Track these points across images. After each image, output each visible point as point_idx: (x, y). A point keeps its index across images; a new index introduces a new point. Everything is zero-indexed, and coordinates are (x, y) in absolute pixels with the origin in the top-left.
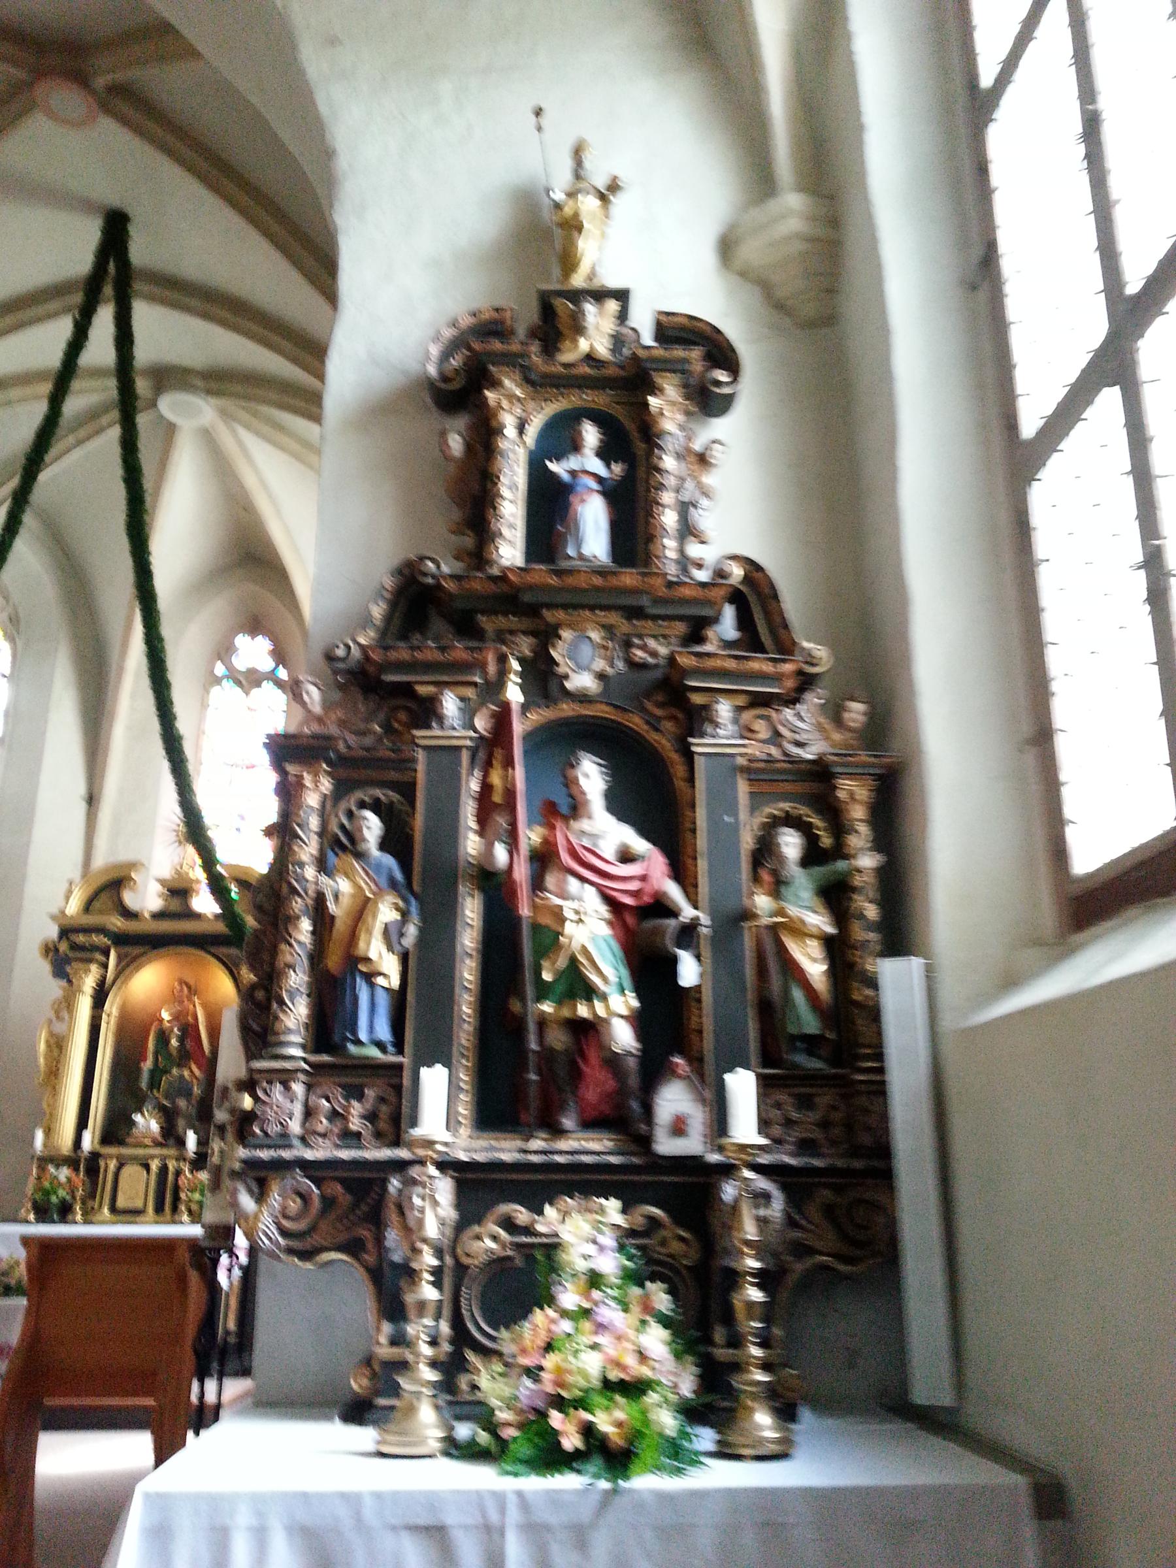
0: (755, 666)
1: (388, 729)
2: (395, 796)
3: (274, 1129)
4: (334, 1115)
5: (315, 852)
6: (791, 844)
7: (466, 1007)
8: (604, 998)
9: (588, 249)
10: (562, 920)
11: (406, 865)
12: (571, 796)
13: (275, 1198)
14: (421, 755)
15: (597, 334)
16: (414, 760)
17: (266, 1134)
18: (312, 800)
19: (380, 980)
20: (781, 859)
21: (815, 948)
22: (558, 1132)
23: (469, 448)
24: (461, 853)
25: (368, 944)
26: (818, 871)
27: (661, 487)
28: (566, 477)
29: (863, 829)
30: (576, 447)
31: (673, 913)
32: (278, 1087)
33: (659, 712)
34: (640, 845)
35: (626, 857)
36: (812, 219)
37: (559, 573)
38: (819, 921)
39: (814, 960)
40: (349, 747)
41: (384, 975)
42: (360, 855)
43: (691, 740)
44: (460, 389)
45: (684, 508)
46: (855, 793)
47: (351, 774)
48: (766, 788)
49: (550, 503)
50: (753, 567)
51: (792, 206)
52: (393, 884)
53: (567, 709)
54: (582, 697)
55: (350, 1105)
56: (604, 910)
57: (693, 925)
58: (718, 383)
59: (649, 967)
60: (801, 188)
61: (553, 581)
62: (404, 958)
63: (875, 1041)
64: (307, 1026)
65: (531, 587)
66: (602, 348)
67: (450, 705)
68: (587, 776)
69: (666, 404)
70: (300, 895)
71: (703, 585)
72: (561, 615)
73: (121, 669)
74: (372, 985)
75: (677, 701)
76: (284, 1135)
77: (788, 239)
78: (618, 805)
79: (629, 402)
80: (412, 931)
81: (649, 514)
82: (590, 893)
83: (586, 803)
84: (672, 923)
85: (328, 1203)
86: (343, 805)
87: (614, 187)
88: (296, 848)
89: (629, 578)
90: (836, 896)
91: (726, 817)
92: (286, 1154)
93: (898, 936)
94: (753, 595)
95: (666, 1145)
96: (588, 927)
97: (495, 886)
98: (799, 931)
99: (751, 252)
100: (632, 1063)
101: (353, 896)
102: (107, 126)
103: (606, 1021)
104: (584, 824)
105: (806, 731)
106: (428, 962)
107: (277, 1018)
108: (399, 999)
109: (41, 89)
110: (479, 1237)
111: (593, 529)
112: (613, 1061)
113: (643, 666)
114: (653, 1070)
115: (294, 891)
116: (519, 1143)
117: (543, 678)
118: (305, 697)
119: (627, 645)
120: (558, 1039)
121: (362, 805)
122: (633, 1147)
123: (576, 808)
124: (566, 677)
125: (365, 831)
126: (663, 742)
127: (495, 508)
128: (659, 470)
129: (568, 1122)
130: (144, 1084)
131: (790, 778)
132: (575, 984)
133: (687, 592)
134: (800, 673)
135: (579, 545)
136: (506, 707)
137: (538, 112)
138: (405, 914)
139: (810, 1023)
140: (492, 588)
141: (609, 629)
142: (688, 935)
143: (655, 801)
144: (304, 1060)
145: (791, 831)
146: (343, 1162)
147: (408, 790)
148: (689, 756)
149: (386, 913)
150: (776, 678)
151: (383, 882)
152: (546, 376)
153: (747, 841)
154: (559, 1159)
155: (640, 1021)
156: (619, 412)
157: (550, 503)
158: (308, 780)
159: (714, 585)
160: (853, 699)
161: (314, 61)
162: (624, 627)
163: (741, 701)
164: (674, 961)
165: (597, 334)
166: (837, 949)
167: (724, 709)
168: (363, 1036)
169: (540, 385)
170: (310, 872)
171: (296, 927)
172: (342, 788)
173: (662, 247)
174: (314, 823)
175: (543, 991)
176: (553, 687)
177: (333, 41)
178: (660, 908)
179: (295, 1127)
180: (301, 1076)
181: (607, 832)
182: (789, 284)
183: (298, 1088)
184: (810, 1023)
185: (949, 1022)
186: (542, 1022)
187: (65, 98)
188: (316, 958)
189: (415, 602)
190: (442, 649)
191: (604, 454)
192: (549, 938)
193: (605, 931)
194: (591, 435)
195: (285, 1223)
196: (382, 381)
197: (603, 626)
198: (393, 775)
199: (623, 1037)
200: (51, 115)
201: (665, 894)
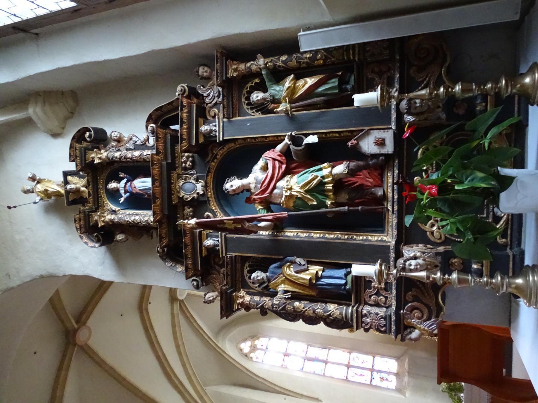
0: (185, 116)
1: (222, 266)
2: (247, 265)
3: (383, 322)
4: (378, 294)
5: (269, 298)
6: (257, 96)
7: (330, 236)
8: (323, 177)
9: (53, 187)
10: (291, 196)
11: (274, 261)
12: (242, 192)
13: (414, 322)
14: (229, 255)
15: (78, 183)
16: (231, 257)
17: (385, 326)
18: (248, 298)
19: (320, 273)
20: (264, 99)
21: (301, 82)
22: (385, 197)
23: (122, 232)
24: (267, 238)
25: (304, 279)
26: (268, 84)
27: (125, 158)
28: (128, 194)
29: (248, 65)
30: (117, 190)
31: (288, 146)
32: (364, 319)
33: (210, 155)
34: (261, 163)
35: (265, 168)
36: (36, 103)
37: (155, 198)
38: (288, 82)
39: (306, 83)
40: (227, 284)
41: (317, 272)
42: (269, 280)
43: (218, 141)
44: (104, 235)
45: (137, 147)
46: (236, 69)
47: (238, 282)
48: (236, 108)
49: (137, 201)
50: (149, 120)
51: (33, 111)
52: (280, 267)
53: (210, 194)
54: (206, 187)
55: (374, 287)
56: (287, 178)
57: (292, 138)
58: (90, 136)
59: (312, 156)
60: (27, 109)
61: (158, 202)
62: (309, 263)
63: (341, 51)
64: (339, 304)
65: (162, 210)
66: (84, 181)
67: (209, 242)
68: (232, 186)
69: (98, 156)
70: (286, 306)
71: (157, 140)
72: (174, 197)
74: (322, 277)
75: (205, 147)
76: (385, 318)
77: (45, 113)
78: (245, 173)
79: (98, 171)
80: (298, 260)
81: (137, 161)
82: (280, 184)
83: (243, 186)
84: (292, 147)
85: (415, 299)
86: (251, 285)
87: (33, 179)
88: (267, 307)
89: (155, 171)
90: (278, 75)
91: (249, 125)
92: (393, 318)
93: (290, 45)
94: (162, 119)
95: (389, 149)
96: (295, 184)
97: (278, 225)
98: (292, 90)
99: (54, 125)
100: (353, 164)
101: (285, 284)
102: (90, 323)
103: (333, 176)
104: (252, 186)
105: (212, 93)
106: (312, 253)
107: (336, 317)
108: (327, 266)
109: (79, 343)
110: (432, 233)
111: (143, 184)
112: (352, 172)
113: (193, 162)
114: (356, 154)
115: (284, 308)
116: (390, 213)
117: (198, 205)
118: (211, 299)
119: (185, 169)
120: (344, 197)
121: (250, 278)
122: (391, 162)
123: (246, 189)
124: (198, 193)
125: (259, 278)
126: (220, 153)
127: (138, 223)
128: (120, 158)
129: (380, 193)
131: (231, 99)
132: (318, 189)
133: (161, 146)
134: (188, 97)
135: (150, 189)
136: (198, 225)
137: (9, 208)
138: (293, 263)
139: (334, 82)
140: (165, 225)
141: (179, 177)
142: (296, 140)
143: (243, 156)
144: (353, 307)
145: (251, 98)
146: (397, 293)
147: (244, 259)
148: (226, 142)
149: (290, 271)
150: (190, 105)
151: (279, 271)
152: (94, 203)
153: (258, 115)
154: (396, 197)
155: (335, 160)
156: (105, 174)
157: (137, 201)
158: (240, 301)
159: (157, 134)
160: (198, 72)
161: (15, 282)
162: (179, 171)
163: (201, 120)
164: (308, 145)
165: (78, 183)
166: (301, 73)
167: (204, 128)
168: (343, 282)
169: (98, 206)
170: (276, 301)
171: (298, 308)
172: (245, 286)
173: (49, 160)
174: (257, 298)
175: (322, 205)
176: (202, 199)
177: (8, 275)
178: (286, 152)
179: (382, 312)
180: (361, 307)
181: (256, 176)
182: (62, 111)
183: (366, 309)
184: (334, 82)
185: (328, 18)
186: (336, 204)
187: (81, 337)
188: (312, 299)
189: (173, 253)
190: (186, 246)
191: (119, 180)
192: (298, 202)
193: (295, 178)
194: (113, 185)
195: (425, 317)
196: (108, 261)
197: (178, 180)
198: (239, 266)
199: (340, 169)
200: (88, 339)
201: (280, 152)
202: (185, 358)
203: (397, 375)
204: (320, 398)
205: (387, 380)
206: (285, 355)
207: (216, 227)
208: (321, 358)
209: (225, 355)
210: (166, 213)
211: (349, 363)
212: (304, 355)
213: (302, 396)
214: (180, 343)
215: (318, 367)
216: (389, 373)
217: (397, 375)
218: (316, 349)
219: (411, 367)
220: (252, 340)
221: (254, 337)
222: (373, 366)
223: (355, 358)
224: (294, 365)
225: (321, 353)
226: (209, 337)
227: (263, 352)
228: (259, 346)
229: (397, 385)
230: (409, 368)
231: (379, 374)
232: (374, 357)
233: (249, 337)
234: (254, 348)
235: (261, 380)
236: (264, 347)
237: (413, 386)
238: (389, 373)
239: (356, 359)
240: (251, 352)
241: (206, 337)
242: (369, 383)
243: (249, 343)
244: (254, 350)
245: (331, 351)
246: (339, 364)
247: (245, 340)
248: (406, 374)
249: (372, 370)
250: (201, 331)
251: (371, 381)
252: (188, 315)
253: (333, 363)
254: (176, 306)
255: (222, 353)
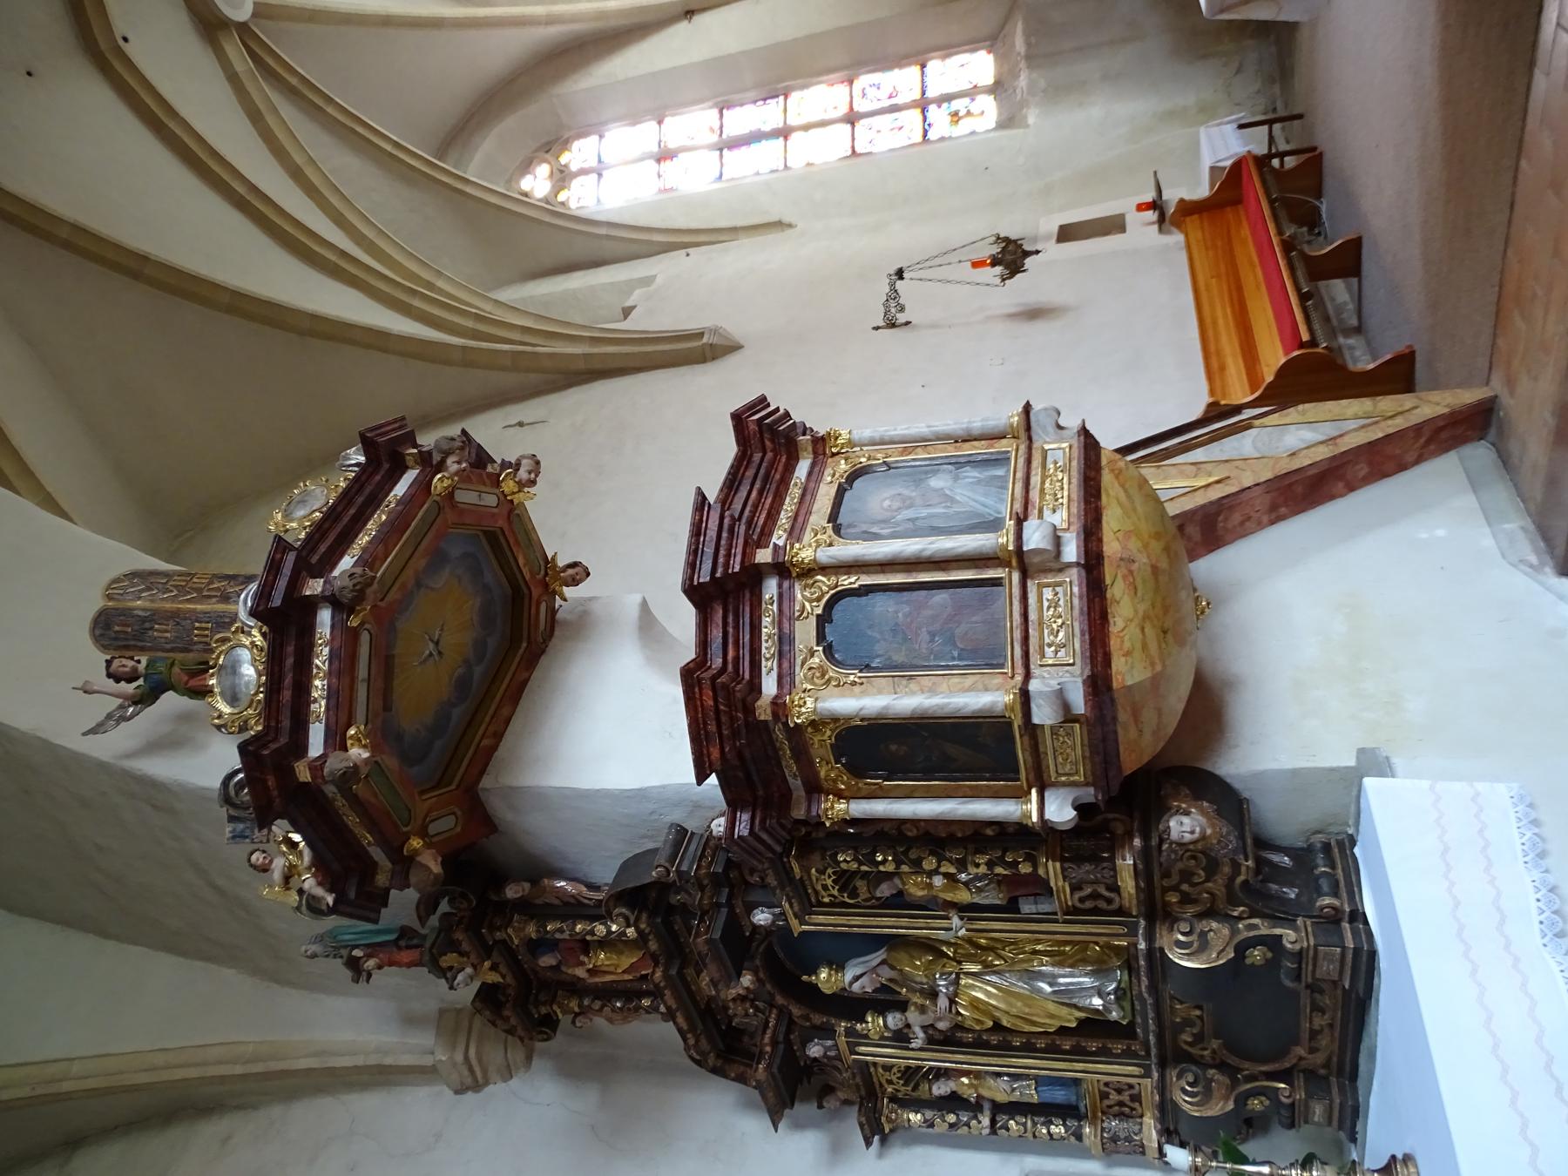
73: (550, 20)
130: (141, 682)
202: (335, 200)
203: (997, 89)
204: (786, 220)
205: (969, 113)
206: (659, 161)
207: (710, 864)
208: (767, 128)
209: (468, 189)
210: (721, 1046)
211: (851, 108)
212: (715, 138)
213: (734, 232)
214: (298, 159)
215: (766, 155)
216: (972, 93)
217: (997, 89)
218: (749, 108)
219: (1033, 40)
220: (547, 156)
221: (552, 144)
222: (923, 93)
223: (869, 91)
224: (695, 176)
225: (767, 115)
226: (397, 145)
227: (595, 176)
228: (574, 168)
229: (1000, 114)
230: (1028, 45)
231: (945, 105)
232: (923, 66)
233: (537, 150)
234: (562, 177)
235: (603, 231)
236: (593, 163)
237: (1044, 91)
238: (972, 93)
239: (871, 92)
240: (557, 189)
241: (389, 148)
242: (920, 139)
243: (543, 170)
244: (563, 180)
245: (795, 96)
246: (823, 124)
247: (526, 167)
248: (1023, 65)
249: (923, 105)
250: (360, 129)
251: (925, 133)
252: (294, 81)
253: (806, 127)
254: (234, 50)
255: (459, 186)
